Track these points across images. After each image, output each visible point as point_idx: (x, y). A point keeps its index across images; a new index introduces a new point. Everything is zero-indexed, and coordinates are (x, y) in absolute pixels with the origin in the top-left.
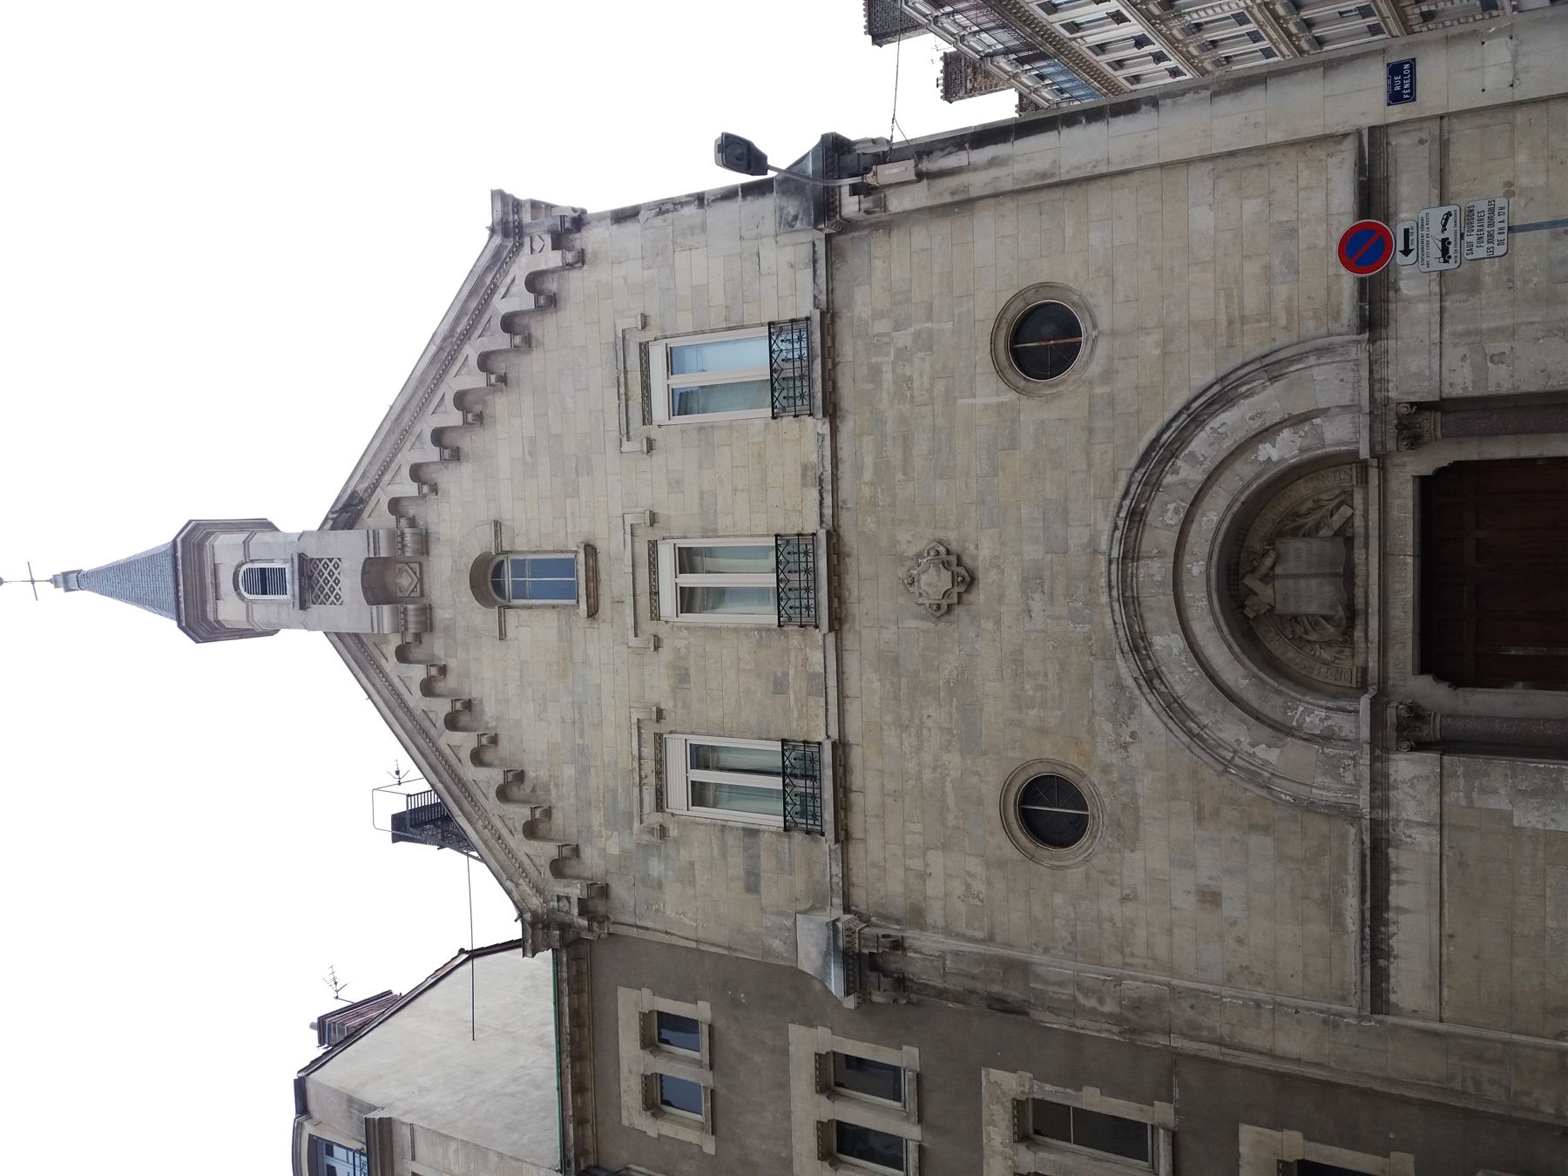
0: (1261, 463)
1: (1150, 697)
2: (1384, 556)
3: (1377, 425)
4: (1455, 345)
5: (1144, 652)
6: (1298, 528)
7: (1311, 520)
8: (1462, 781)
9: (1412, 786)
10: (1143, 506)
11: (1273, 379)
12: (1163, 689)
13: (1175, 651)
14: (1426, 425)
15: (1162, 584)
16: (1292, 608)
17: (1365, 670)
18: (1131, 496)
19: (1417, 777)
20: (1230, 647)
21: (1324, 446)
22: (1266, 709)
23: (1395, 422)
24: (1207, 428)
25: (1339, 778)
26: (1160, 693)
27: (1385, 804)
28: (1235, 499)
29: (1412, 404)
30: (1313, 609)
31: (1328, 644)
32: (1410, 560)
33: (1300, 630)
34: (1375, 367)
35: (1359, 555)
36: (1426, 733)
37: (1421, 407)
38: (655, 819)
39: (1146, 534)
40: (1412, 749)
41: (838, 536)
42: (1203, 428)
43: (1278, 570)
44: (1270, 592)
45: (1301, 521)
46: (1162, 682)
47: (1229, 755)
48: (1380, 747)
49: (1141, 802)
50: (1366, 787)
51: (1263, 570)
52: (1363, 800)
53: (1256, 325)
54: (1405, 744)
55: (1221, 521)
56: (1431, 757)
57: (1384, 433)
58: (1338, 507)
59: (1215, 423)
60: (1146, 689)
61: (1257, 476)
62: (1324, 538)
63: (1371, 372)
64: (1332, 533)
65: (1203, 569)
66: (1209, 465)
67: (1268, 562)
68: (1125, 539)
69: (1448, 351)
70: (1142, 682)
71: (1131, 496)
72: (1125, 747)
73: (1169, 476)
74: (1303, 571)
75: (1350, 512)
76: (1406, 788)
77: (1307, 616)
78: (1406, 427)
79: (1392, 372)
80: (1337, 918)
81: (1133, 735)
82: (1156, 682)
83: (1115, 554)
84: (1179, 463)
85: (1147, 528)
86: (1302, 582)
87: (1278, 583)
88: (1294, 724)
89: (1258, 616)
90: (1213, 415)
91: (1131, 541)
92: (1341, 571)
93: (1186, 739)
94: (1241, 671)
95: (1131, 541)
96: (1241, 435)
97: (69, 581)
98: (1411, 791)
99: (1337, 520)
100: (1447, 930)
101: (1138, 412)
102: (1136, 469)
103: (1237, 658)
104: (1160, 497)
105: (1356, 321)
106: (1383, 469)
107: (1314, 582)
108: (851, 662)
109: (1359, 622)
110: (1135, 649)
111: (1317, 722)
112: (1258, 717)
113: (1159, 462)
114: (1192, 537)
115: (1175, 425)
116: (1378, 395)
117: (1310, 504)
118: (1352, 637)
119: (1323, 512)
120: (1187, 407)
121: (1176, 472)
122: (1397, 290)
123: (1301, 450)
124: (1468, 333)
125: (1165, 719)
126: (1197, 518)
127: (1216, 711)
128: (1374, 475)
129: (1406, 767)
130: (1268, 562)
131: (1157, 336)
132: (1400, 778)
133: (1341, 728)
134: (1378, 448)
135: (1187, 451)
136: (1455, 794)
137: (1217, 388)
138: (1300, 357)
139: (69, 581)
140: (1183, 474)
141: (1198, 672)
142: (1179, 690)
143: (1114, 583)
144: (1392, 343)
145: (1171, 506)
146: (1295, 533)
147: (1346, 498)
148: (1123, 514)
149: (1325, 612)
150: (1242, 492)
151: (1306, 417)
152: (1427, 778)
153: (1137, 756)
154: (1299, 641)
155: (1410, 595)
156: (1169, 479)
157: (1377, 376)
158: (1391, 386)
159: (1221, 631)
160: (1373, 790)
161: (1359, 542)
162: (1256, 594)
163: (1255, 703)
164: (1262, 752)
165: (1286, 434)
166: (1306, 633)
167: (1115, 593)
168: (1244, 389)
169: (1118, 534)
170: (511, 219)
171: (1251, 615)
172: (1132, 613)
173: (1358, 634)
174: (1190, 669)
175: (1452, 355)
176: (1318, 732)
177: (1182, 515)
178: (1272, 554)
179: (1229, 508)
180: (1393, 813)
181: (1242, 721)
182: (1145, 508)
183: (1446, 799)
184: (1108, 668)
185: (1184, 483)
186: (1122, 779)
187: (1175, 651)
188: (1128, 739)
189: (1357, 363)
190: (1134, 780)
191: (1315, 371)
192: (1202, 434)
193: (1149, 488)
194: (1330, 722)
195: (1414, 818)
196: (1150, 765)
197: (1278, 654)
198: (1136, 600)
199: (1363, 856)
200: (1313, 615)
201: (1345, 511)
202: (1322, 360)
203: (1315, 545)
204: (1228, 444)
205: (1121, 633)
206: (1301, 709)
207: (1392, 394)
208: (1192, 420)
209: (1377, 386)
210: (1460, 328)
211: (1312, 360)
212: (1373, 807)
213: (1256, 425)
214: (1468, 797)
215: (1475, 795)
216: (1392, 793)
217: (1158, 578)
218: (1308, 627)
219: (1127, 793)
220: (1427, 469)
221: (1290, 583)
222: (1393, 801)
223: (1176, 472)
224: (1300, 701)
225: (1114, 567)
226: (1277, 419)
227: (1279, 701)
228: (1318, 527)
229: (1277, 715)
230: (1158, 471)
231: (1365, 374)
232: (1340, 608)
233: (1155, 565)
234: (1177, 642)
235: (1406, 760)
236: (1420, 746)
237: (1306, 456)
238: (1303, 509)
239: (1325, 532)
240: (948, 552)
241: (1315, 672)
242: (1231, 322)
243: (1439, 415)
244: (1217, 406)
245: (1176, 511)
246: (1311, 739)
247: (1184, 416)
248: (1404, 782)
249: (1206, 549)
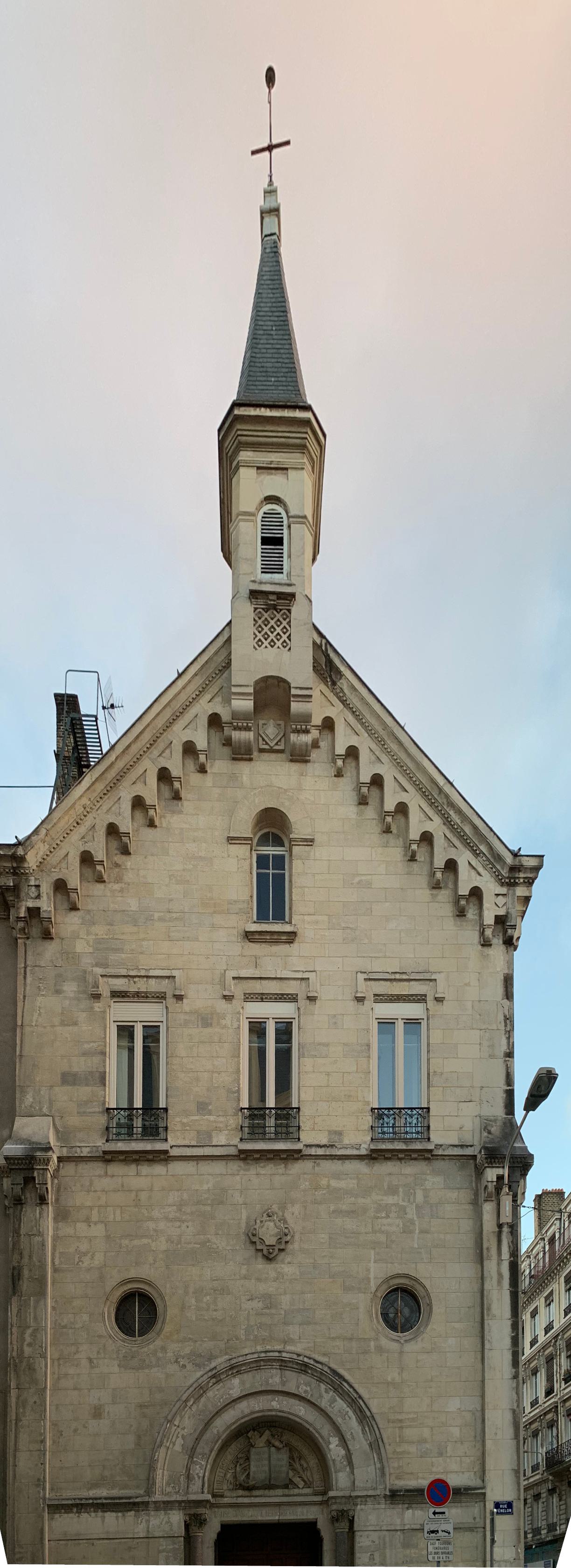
0: (328, 1439)
1: (206, 1377)
2: (279, 1505)
3: (344, 1500)
4: (379, 1538)
5: (230, 1373)
6: (293, 1459)
7: (297, 1466)
8: (171, 1547)
9: (167, 1523)
10: (310, 1372)
11: (370, 1445)
12: (211, 1384)
13: (231, 1392)
14: (343, 1524)
15: (267, 1383)
16: (253, 1457)
17: (222, 1496)
18: (315, 1364)
19: (171, 1525)
20: (234, 1423)
21: (336, 1472)
22: (202, 1444)
23: (345, 1509)
24: (348, 1409)
25: (168, 1484)
26: (208, 1382)
27: (157, 1509)
28: (311, 1425)
29: (353, 1517)
30: (253, 1469)
31: (235, 1477)
32: (277, 1518)
33: (242, 1461)
34: (372, 1498)
35: (279, 1492)
36: (194, 1529)
37: (352, 1522)
38: (105, 992)
39: (294, 1374)
40: (185, 1522)
41: (298, 1159)
42: (348, 1406)
43: (273, 1449)
44: (261, 1445)
45: (297, 1460)
46: (214, 1384)
47: (176, 1423)
48: (183, 1505)
49: (147, 1371)
50: (166, 1499)
51: (273, 1441)
52: (158, 1497)
53: (397, 1435)
54: (188, 1518)
55: (300, 1417)
56: (182, 1531)
57: (340, 1504)
58: (304, 1481)
59: (351, 1413)
60: (210, 1374)
61: (322, 1437)
62: (288, 1473)
63: (370, 1496)
64: (290, 1477)
65: (275, 1408)
66: (329, 1410)
67: (277, 1443)
68: (292, 1361)
69: (377, 1534)
70: (214, 1372)
71: (315, 1364)
72: (176, 1361)
73: (324, 1387)
74: (273, 1462)
75: (301, 1486)
76: (166, 1519)
77: (249, 1465)
78: (342, 1514)
79: (369, 1506)
80: (95, 1485)
81: (184, 1366)
82: (214, 1380)
83: (284, 1355)
84: (331, 1393)
85: (297, 1374)
86: (266, 1462)
87: (266, 1449)
88: (195, 1459)
89: (249, 1438)
90: (355, 1411)
91: (290, 1365)
92: (272, 1483)
93: (184, 1398)
94: (221, 1430)
95: (290, 1365)
96: (343, 1428)
97: (271, 212)
98: (164, 1523)
99: (297, 1480)
100: (96, 1542)
101: (359, 1369)
102: (329, 1368)
103: (229, 1427)
104: (314, 1382)
105: (395, 1488)
106: (321, 1503)
107: (267, 1468)
108: (218, 1167)
109: (246, 1493)
110: (232, 1368)
111: (197, 1472)
112: (198, 1440)
113: (332, 1381)
114: (292, 1401)
115: (351, 1390)
116: (359, 1500)
117: (305, 1465)
118: (239, 1489)
119: (301, 1472)
120: (360, 1397)
121: (326, 1392)
122: (408, 1509)
123: (334, 1461)
124: (385, 1544)
125: (195, 1386)
126: (302, 1404)
127: (200, 1415)
128: (319, 1498)
129: (177, 1518)
130: (277, 1443)
131: (398, 1379)
132: (170, 1516)
133: (194, 1484)
134: (334, 1501)
135: (337, 1398)
136: (164, 1544)
137: (368, 1413)
138: (380, 1459)
139: (271, 212)
140: (325, 1395)
141: (220, 1405)
142: (210, 1394)
143: (269, 1354)
144: (383, 1506)
145: (308, 1389)
146: (292, 1458)
147: (307, 1485)
148: (306, 1360)
149: (251, 1474)
150: (315, 1428)
151: (350, 1463)
152: (171, 1530)
153: (172, 1368)
154: (236, 1462)
155: (260, 1518)
156: (323, 1386)
157: (368, 1499)
158: (363, 1507)
159: (242, 1418)
160: (164, 1502)
161: (286, 1491)
162: (260, 1437)
163: (205, 1437)
164: (180, 1441)
165: (343, 1452)
166: (240, 1465)
167: (263, 1355)
168: (367, 1429)
169: (295, 1357)
170: (522, 875)
171: (249, 1435)
172: (252, 1366)
173: (241, 1492)
174: (221, 1400)
175: (374, 1536)
176: (191, 1472)
177: (303, 1395)
178: (281, 1446)
179: (307, 1422)
180: (152, 1513)
181: (195, 1430)
182: (308, 1373)
183: (161, 1540)
184: (221, 1351)
185: (321, 1396)
186: (159, 1359)
187: (231, 1392)
188: (181, 1363)
189: (375, 1489)
190: (159, 1366)
191: (373, 1467)
192: (345, 1406)
193: (319, 1375)
194: (197, 1478)
195: (151, 1523)
196: (168, 1376)
197: (229, 1450)
198: (258, 1368)
199: (130, 1498)
200: (249, 1468)
201: (301, 1484)
202: (378, 1471)
203: (284, 1469)
204: (339, 1420)
205: (241, 1359)
206: (203, 1463)
207: (359, 1506)
208: (353, 1400)
209: (364, 1500)
210: (387, 1539)
211: (378, 1465)
212: (155, 1502)
213: (348, 1436)
214: (163, 1551)
215: (164, 1554)
216: (163, 1512)
217: (271, 1381)
218: (243, 1466)
219: (151, 1362)
220: (320, 1525)
221: (266, 1456)
222: (159, 1513)
223: (326, 1392)
224: (207, 1462)
225: (277, 1354)
226: (350, 1447)
227: (207, 1451)
228: (294, 1470)
229: (199, 1450)
230: (328, 1381)
231: (370, 1493)
232: (254, 1482)
233: (277, 1379)
234: (236, 1393)
235: (180, 1519)
236: (187, 1526)
237: (331, 1463)
238: (303, 1462)
239: (291, 1474)
240: (287, 1242)
241: (221, 1470)
242: (401, 1421)
243: (347, 1530)
244: (359, 1414)
245: (306, 1392)
246: (188, 1469)
247: (355, 1395)
248: (169, 1518)
249: (285, 1409)
